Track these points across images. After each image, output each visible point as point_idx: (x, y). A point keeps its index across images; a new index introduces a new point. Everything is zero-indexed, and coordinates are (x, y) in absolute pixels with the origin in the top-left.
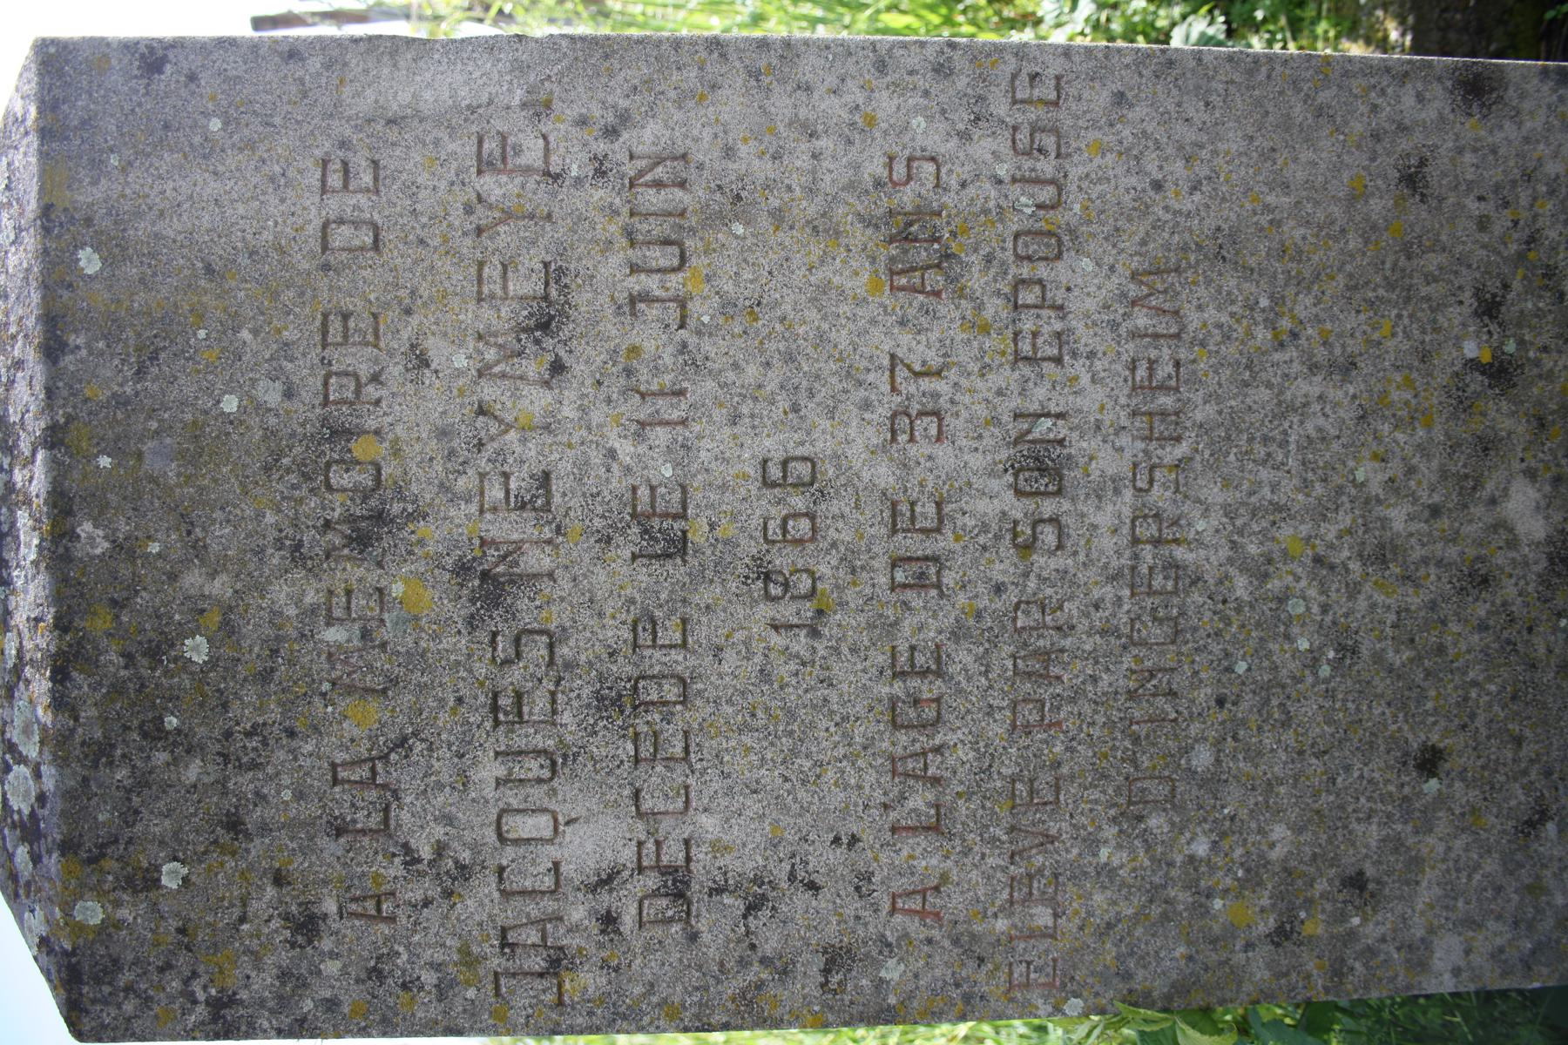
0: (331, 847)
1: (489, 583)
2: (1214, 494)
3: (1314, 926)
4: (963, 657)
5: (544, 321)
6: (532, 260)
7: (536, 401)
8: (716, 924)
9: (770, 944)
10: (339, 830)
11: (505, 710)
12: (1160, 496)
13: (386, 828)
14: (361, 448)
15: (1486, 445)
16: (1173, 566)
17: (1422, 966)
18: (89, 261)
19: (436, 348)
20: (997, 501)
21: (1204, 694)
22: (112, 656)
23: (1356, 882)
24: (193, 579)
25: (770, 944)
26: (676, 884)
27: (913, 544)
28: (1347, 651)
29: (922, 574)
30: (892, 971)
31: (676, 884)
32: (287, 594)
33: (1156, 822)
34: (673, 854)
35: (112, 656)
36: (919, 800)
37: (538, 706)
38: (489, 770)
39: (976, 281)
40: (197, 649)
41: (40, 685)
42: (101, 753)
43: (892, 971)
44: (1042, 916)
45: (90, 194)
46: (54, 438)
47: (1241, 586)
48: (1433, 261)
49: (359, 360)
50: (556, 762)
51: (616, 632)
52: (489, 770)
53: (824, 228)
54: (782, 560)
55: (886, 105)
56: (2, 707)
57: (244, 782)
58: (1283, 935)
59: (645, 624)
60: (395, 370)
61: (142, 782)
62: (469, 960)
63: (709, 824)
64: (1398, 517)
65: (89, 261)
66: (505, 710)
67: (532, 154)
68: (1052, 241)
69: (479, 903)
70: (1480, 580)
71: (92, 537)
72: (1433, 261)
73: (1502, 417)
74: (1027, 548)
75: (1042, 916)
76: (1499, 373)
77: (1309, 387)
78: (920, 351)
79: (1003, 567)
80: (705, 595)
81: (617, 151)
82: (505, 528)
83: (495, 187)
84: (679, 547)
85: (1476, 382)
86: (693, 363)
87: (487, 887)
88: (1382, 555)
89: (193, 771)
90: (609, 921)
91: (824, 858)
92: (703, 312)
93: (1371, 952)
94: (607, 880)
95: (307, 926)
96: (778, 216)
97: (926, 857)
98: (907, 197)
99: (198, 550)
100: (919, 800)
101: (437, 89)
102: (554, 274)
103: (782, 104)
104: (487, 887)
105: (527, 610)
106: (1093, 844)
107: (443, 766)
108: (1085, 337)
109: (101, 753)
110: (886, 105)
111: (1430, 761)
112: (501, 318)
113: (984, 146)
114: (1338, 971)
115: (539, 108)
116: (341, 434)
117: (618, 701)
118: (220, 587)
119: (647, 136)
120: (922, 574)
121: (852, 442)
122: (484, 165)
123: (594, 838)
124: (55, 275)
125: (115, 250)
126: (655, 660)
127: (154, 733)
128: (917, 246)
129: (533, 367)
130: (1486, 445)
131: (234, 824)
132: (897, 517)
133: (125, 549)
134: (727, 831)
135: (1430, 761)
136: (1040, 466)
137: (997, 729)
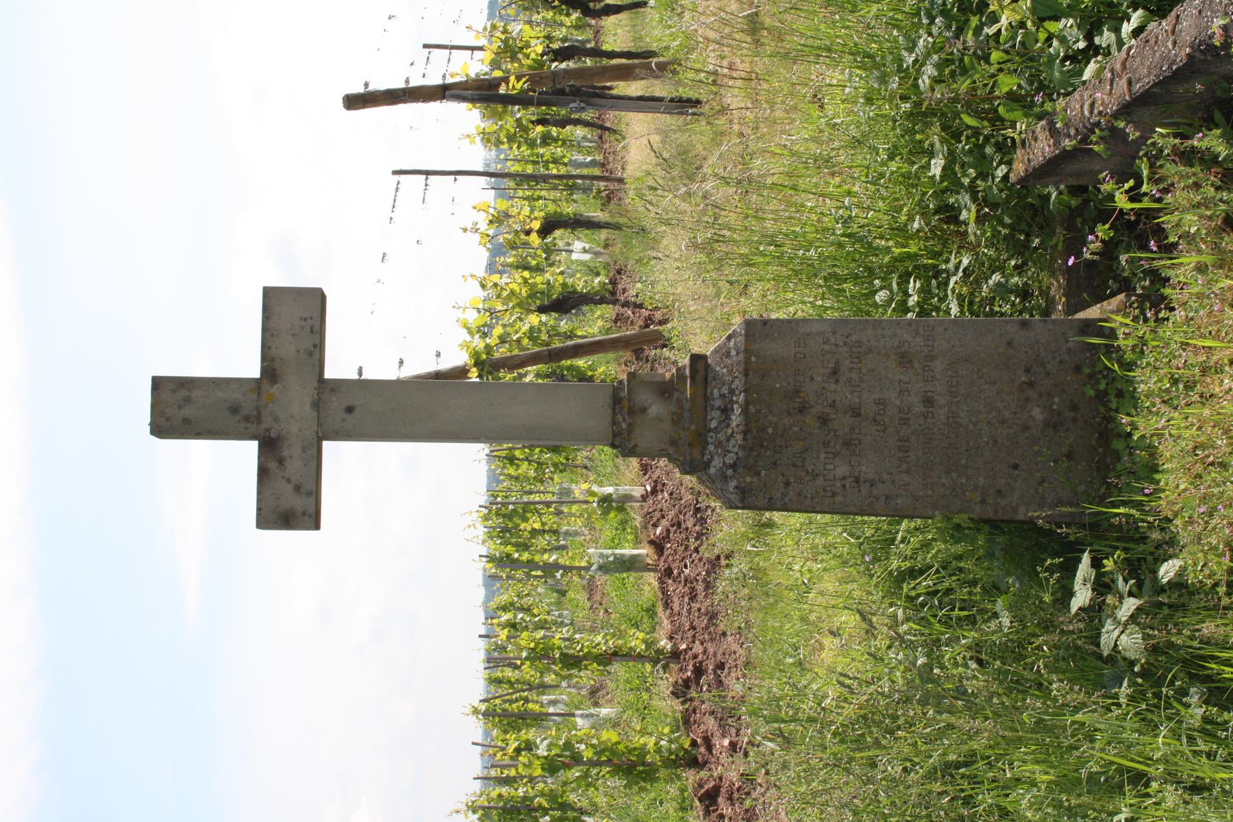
0: (793, 469)
1: (824, 420)
2: (965, 408)
3: (990, 501)
4: (913, 439)
5: (835, 372)
6: (833, 361)
7: (833, 387)
8: (864, 488)
9: (875, 493)
10: (795, 466)
11: (826, 444)
12: (953, 408)
13: (803, 466)
14: (802, 395)
15: (1027, 399)
16: (957, 423)
17: (1016, 512)
18: (753, 359)
19: (815, 377)
20: (920, 408)
21: (963, 449)
22: (755, 431)
23: (999, 492)
24: (770, 417)
25: (875, 493)
26: (857, 480)
27: (902, 416)
28: (995, 442)
29: (905, 422)
30: (899, 501)
31: (857, 480)
32: (787, 421)
33: (954, 475)
34: (857, 474)
35: (755, 431)
36: (904, 466)
37: (832, 444)
38: (823, 456)
39: (916, 366)
40: (770, 430)
41: (739, 437)
42: (752, 449)
43: (899, 501)
44: (930, 492)
45: (754, 347)
46: (746, 391)
47: (971, 427)
48: (1014, 361)
49: (801, 378)
50: (836, 454)
51: (847, 430)
52: (823, 456)
53: (887, 355)
54: (878, 418)
55: (899, 332)
56: (1229, 79)
57: (777, 456)
58: (983, 502)
59: (852, 429)
60: (808, 380)
61: (759, 455)
62: (817, 493)
63: (864, 468)
64: (1007, 414)
65: (753, 359)
66: (826, 444)
67: (833, 340)
68: (932, 358)
69: (820, 481)
70: (1026, 428)
71: (752, 409)
72: (1014, 361)
73: (1031, 393)
74: (926, 418)
75: (930, 492)
76: (1030, 384)
77: (985, 387)
78: (905, 379)
79: (921, 421)
80: (864, 424)
81: (848, 340)
82: (827, 410)
83: (826, 347)
84: (859, 415)
85: (1025, 386)
86: (862, 381)
87: (821, 478)
88: (1003, 422)
89: (768, 453)
90: (844, 486)
91: (886, 477)
92: (864, 371)
93: (1003, 508)
94: (844, 478)
95: (787, 484)
96: (878, 353)
97: (906, 478)
98: (903, 349)
99: (771, 412)
100: (904, 466)
101: (815, 328)
102: (837, 363)
103: (879, 332)
104: (821, 478)
105: (830, 425)
106: (940, 478)
107: (814, 455)
108: (938, 377)
109: (752, 449)
110: (899, 332)
111: (1016, 467)
112: (827, 371)
113: (918, 339)
114: (996, 511)
115: (834, 333)
116: (798, 392)
117: (847, 444)
118: (775, 419)
119: (854, 338)
120: (905, 422)
121: (892, 396)
122: (824, 343)
123: (842, 470)
124: (747, 362)
125: (757, 357)
126: (855, 436)
127: (762, 446)
128: (904, 359)
129: (833, 380)
130: (1027, 399)
131: (775, 464)
132: (900, 410)
133: (758, 411)
134: (867, 470)
135: (1016, 467)
136: (928, 402)
137: (920, 453)
